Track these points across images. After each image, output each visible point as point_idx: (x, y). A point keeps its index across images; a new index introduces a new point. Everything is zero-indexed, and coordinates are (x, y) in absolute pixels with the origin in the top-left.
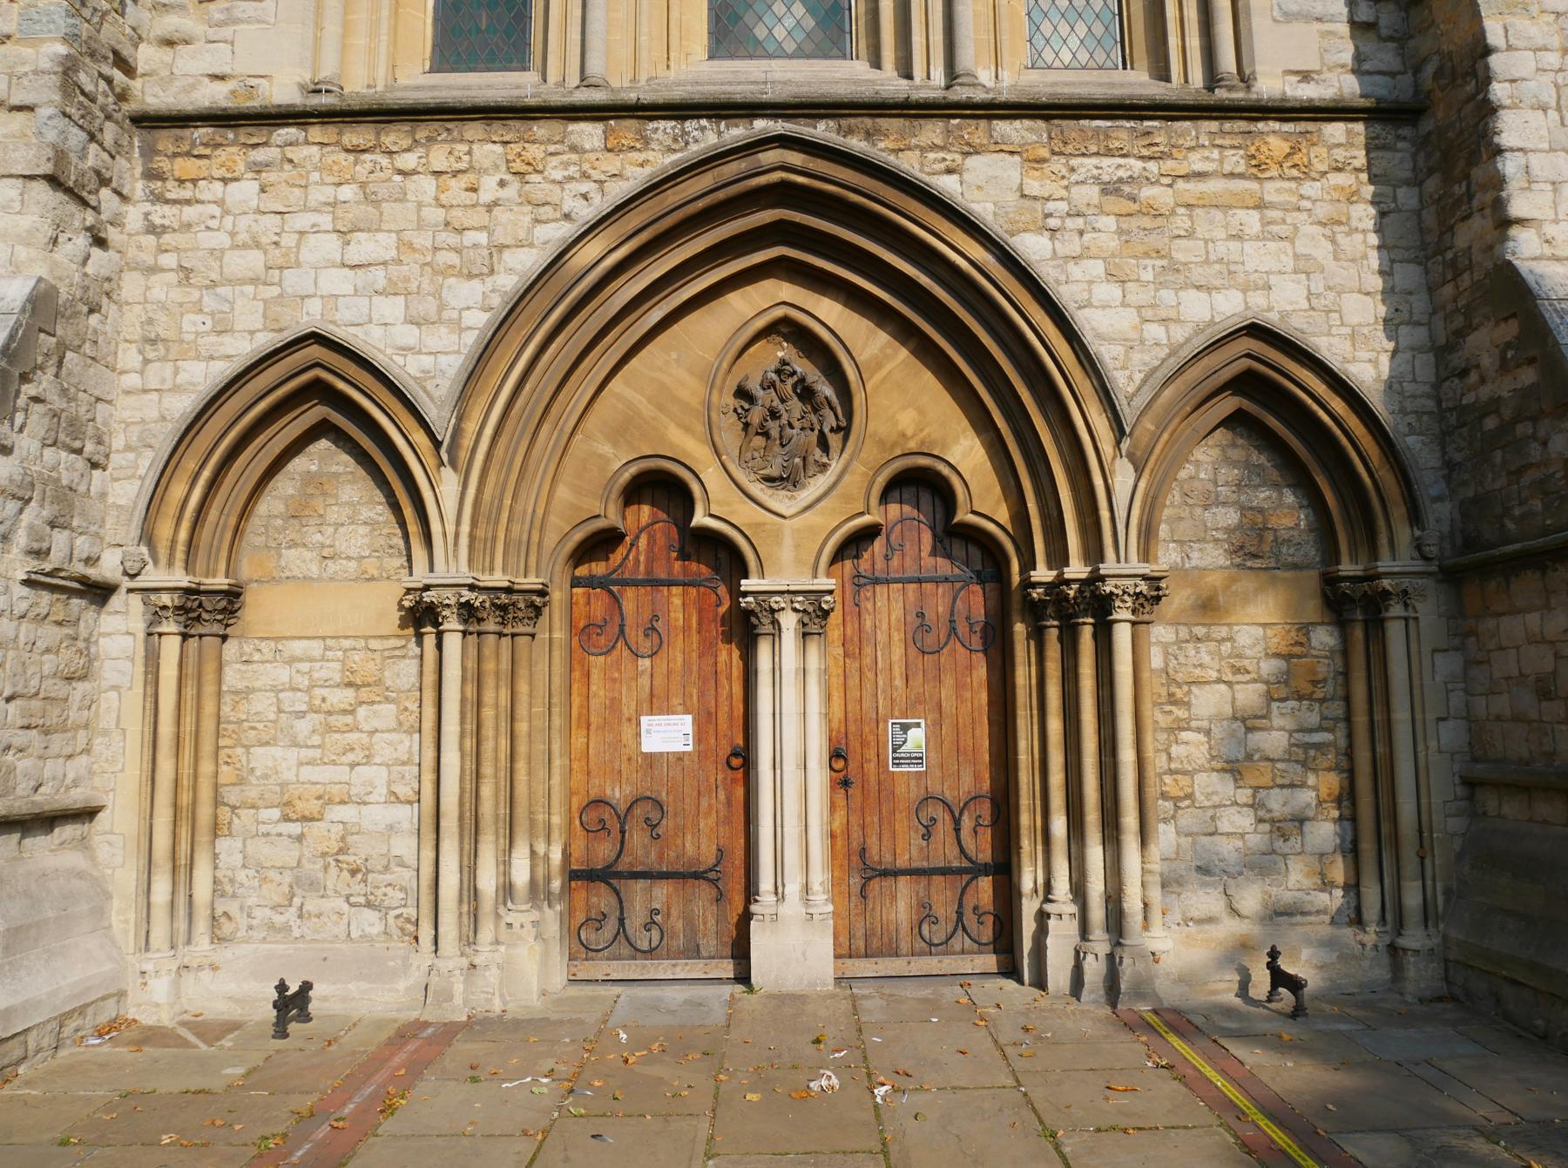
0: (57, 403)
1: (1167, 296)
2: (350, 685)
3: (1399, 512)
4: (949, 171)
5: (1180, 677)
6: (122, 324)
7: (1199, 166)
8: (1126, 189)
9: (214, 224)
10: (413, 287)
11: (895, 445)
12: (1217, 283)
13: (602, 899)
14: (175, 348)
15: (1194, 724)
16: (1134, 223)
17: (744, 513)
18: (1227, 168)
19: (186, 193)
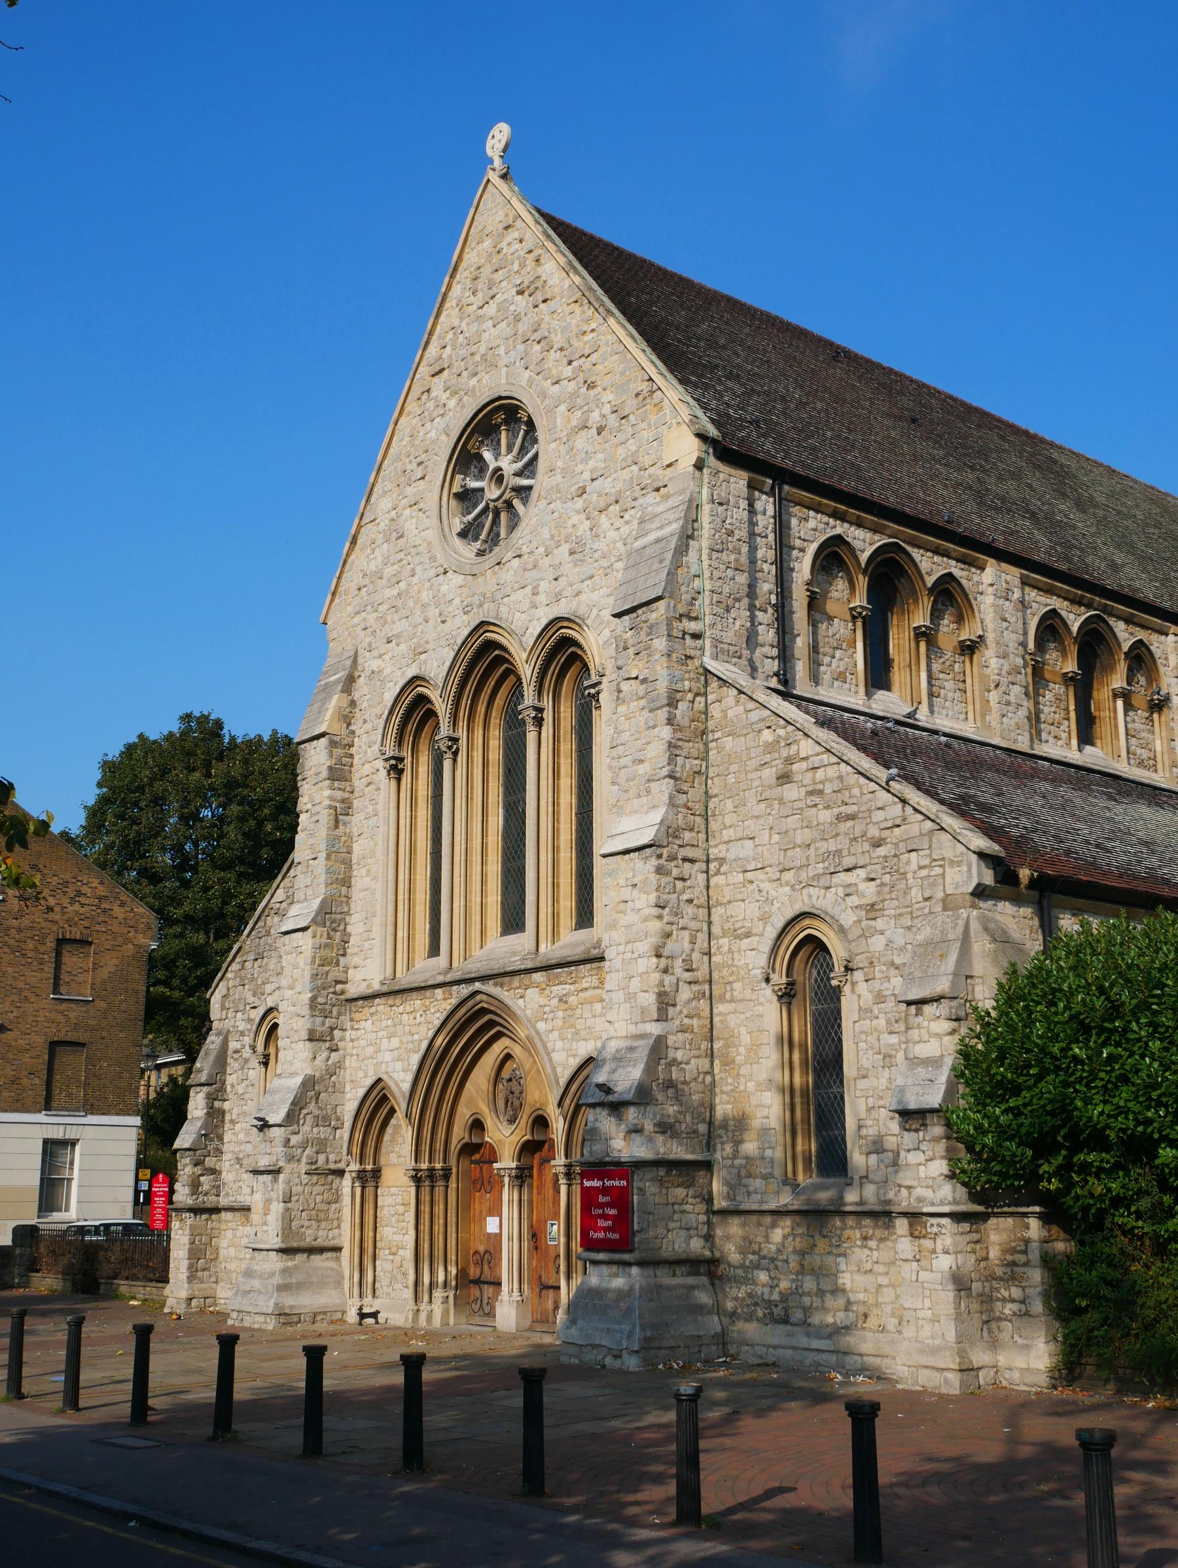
0: (317, 1112)
6: (347, 1074)
7: (585, 985)
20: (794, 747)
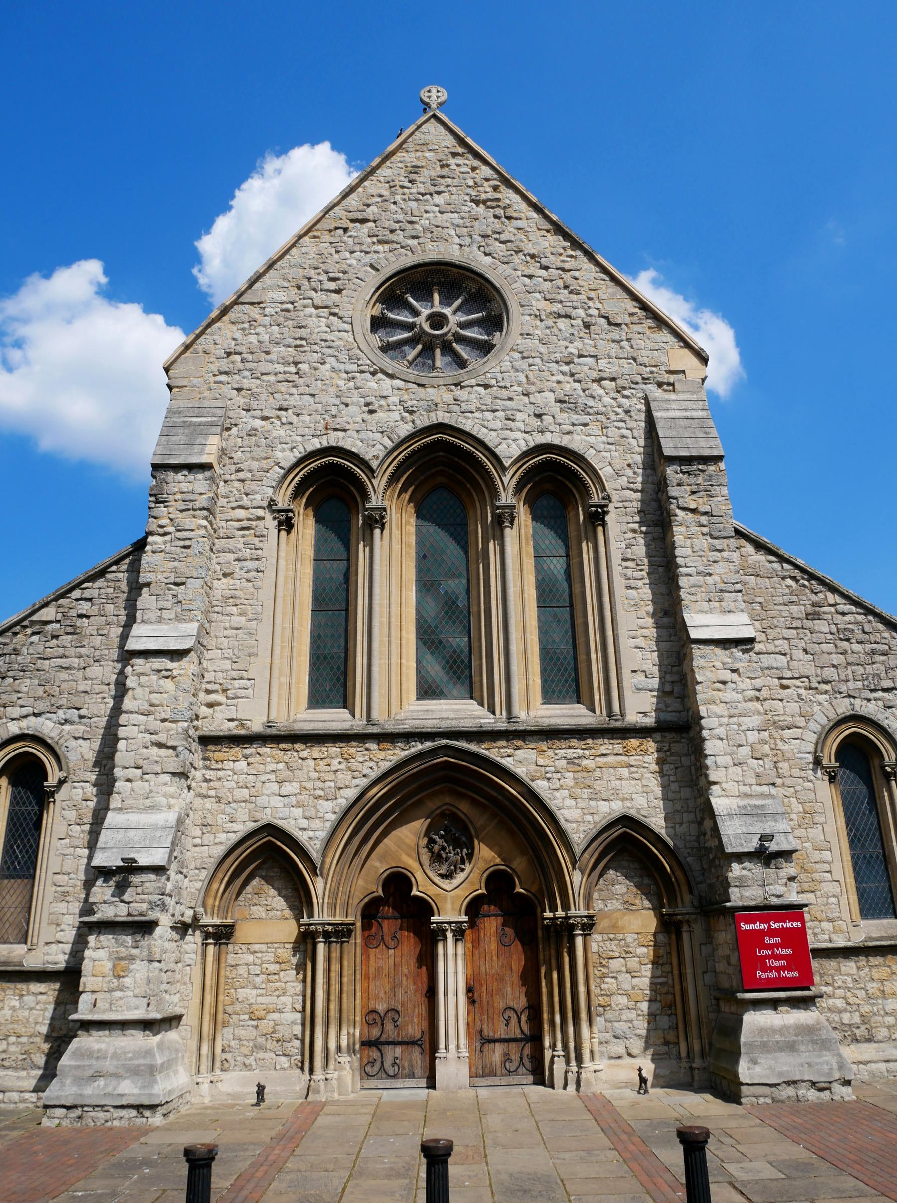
1: (593, 803)
2: (277, 962)
3: (685, 888)
4: (509, 756)
5: (604, 956)
7: (604, 752)
8: (576, 761)
9: (229, 778)
10: (306, 804)
11: (490, 861)
12: (612, 798)
13: (374, 1054)
14: (214, 828)
15: (611, 975)
16: (580, 775)
17: (432, 890)
18: (615, 752)
19: (219, 766)
20: (821, 595)
